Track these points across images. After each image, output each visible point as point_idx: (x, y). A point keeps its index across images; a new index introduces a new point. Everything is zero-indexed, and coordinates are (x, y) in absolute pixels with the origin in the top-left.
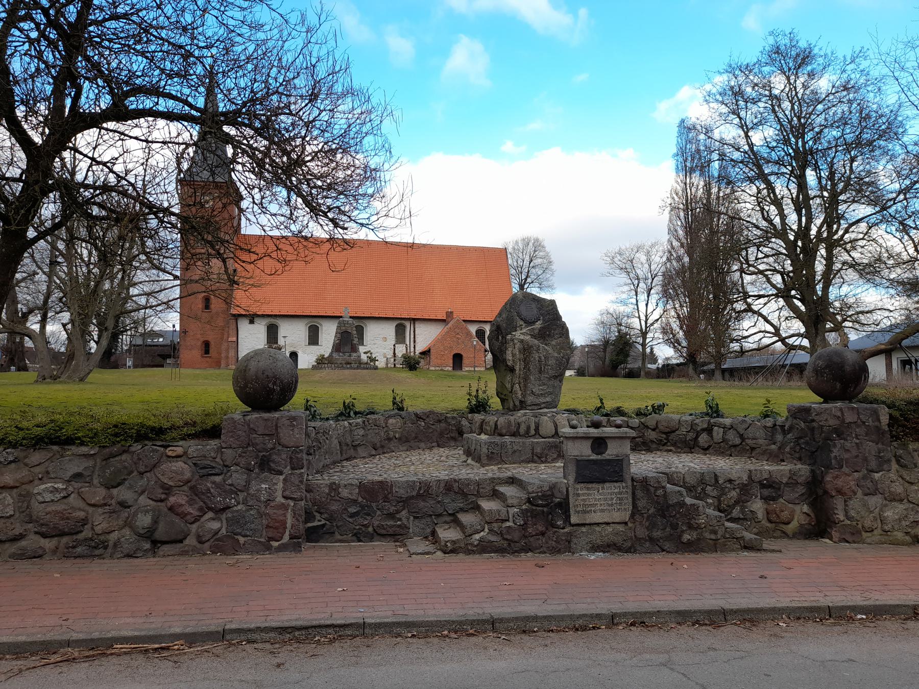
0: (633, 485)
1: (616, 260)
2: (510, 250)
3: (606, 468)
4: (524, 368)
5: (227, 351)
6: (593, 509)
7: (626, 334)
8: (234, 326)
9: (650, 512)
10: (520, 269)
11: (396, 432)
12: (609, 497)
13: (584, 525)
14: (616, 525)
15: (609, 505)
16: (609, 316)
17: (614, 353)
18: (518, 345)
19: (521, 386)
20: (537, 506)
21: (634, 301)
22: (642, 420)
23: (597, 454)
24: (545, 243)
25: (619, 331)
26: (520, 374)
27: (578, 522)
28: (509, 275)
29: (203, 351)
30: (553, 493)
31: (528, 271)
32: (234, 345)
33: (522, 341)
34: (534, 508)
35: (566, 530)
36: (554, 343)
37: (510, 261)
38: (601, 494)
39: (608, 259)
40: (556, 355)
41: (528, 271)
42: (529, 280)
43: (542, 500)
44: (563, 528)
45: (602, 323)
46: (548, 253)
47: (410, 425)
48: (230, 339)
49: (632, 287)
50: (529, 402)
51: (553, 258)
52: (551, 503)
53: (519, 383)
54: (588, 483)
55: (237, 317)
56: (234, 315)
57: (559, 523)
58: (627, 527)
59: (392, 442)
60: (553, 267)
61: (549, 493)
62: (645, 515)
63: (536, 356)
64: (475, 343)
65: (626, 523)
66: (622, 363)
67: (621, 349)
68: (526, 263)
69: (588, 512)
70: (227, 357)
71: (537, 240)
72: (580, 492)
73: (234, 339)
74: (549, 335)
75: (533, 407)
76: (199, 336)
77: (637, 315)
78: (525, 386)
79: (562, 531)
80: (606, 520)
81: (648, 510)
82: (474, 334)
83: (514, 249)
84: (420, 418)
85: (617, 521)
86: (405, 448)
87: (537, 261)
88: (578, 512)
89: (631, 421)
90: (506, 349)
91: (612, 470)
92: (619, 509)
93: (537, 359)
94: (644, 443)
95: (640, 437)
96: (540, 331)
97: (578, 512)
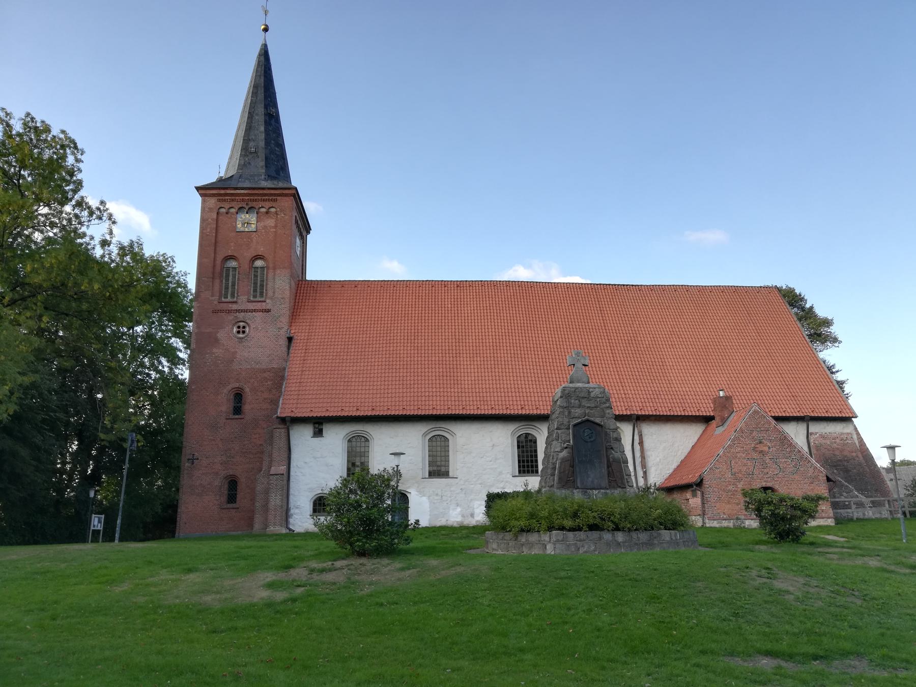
8: (282, 443)
29: (224, 499)
48: (273, 470)
56: (283, 420)
73: (283, 469)
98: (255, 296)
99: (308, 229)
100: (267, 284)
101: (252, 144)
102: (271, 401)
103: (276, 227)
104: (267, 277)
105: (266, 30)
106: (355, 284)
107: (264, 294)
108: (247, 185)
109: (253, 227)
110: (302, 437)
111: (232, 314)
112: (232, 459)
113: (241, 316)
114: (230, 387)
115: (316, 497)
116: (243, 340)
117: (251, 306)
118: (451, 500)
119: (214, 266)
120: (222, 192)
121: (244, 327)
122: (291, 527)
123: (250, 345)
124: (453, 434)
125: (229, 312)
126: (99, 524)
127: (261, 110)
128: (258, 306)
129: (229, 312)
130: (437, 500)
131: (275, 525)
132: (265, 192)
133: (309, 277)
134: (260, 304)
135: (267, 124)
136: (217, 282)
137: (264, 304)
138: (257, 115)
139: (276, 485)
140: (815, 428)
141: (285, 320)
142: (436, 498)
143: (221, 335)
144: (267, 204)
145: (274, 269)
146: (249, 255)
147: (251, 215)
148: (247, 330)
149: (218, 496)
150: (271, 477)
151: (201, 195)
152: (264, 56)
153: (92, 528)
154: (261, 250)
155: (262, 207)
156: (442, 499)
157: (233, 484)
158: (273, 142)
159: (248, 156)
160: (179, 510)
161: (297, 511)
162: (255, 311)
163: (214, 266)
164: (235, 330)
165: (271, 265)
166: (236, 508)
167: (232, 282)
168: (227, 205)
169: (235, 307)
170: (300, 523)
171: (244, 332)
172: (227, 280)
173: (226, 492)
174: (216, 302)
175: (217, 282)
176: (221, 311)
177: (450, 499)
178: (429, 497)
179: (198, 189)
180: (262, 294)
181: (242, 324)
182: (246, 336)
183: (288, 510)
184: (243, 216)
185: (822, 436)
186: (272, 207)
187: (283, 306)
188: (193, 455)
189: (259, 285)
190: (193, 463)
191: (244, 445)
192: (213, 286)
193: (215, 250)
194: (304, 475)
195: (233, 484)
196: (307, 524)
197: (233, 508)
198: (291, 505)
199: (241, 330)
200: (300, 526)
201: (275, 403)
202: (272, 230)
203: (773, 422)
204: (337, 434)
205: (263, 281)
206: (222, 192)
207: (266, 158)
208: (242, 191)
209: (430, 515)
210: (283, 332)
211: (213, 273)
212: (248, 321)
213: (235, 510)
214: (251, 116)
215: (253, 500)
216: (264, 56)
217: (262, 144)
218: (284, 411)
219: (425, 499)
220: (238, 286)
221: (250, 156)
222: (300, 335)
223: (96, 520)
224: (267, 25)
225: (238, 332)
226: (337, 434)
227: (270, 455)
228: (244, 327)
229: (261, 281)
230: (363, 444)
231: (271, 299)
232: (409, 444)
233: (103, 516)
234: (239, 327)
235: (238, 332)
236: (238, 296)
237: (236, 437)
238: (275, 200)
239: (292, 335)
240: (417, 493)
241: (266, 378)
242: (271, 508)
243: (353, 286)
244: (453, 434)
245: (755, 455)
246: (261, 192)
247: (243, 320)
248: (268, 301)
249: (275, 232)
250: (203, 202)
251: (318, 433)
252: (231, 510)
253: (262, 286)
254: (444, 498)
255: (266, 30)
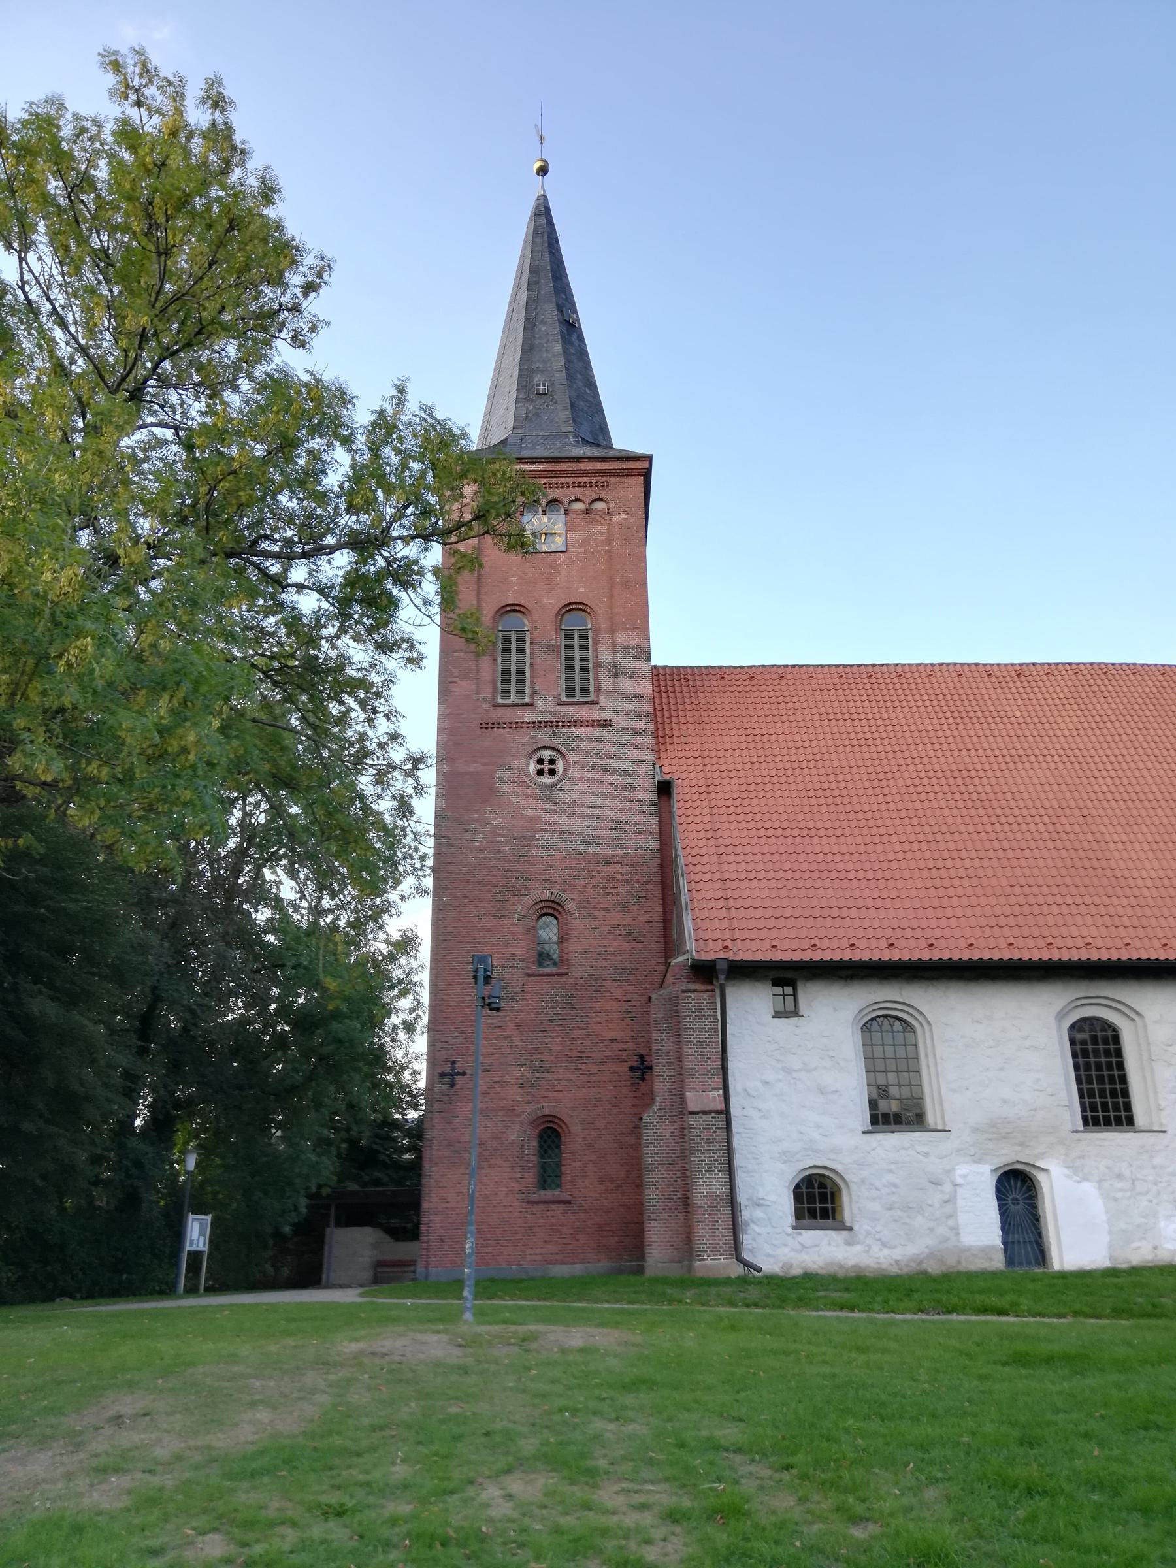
29: (531, 1177)
98: (570, 693)
100: (597, 666)
102: (630, 933)
103: (609, 541)
104: (595, 650)
105: (543, 171)
106: (781, 673)
107: (592, 689)
108: (540, 452)
111: (524, 730)
112: (547, 1076)
113: (544, 735)
114: (529, 899)
115: (801, 1176)
116: (554, 790)
117: (567, 713)
118: (1159, 1193)
121: (552, 761)
122: (747, 1256)
123: (569, 800)
124: (1133, 1016)
125: (518, 726)
126: (202, 1238)
127: (549, 312)
128: (583, 713)
129: (518, 726)
130: (1121, 1190)
131: (715, 1251)
132: (582, 466)
134: (585, 708)
137: (595, 707)
138: (543, 322)
139: (708, 1142)
141: (646, 743)
142: (1120, 1185)
143: (501, 778)
144: (588, 494)
145: (613, 631)
146: (555, 601)
147: (554, 518)
148: (560, 766)
149: (518, 1169)
150: (692, 1119)
152: (543, 215)
153: (188, 1248)
155: (577, 500)
156: (1133, 1189)
158: (579, 376)
159: (532, 401)
160: (425, 1205)
161: (759, 1213)
162: (575, 724)
164: (533, 767)
165: (604, 625)
166: (564, 1202)
167: (518, 662)
169: (529, 715)
170: (768, 1249)
171: (552, 772)
173: (534, 1159)
174: (486, 706)
176: (500, 725)
177: (1155, 1189)
178: (1100, 1181)
180: (585, 690)
181: (547, 754)
182: (560, 781)
183: (734, 1207)
186: (599, 500)
187: (639, 713)
188: (453, 1063)
189: (577, 668)
190: (453, 1085)
191: (573, 1040)
192: (478, 671)
193: (478, 593)
194: (763, 1117)
196: (786, 1250)
197: (559, 1202)
198: (742, 1197)
199: (546, 767)
200: (769, 1256)
202: (600, 548)
204: (835, 1010)
205: (587, 659)
207: (572, 405)
208: (533, 467)
209: (1110, 1233)
210: (643, 772)
212: (560, 747)
213: (562, 1207)
214: (530, 325)
216: (543, 215)
217: (560, 376)
219: (1088, 1188)
220: (532, 670)
221: (539, 402)
223: (196, 1226)
224: (545, 161)
225: (540, 773)
226: (835, 1010)
228: (552, 761)
229: (581, 660)
230: (900, 1038)
231: (609, 695)
232: (1026, 1038)
233: (209, 1218)
234: (540, 761)
235: (540, 773)
236: (534, 692)
237: (551, 1021)
238: (605, 485)
239: (667, 777)
240: (1067, 1172)
241: (613, 877)
242: (700, 1203)
243: (776, 676)
244: (1133, 1016)
246: (574, 466)
247: (549, 744)
248: (603, 702)
249: (609, 551)
252: (554, 1207)
253: (585, 671)
254: (1140, 1187)
255: (543, 171)
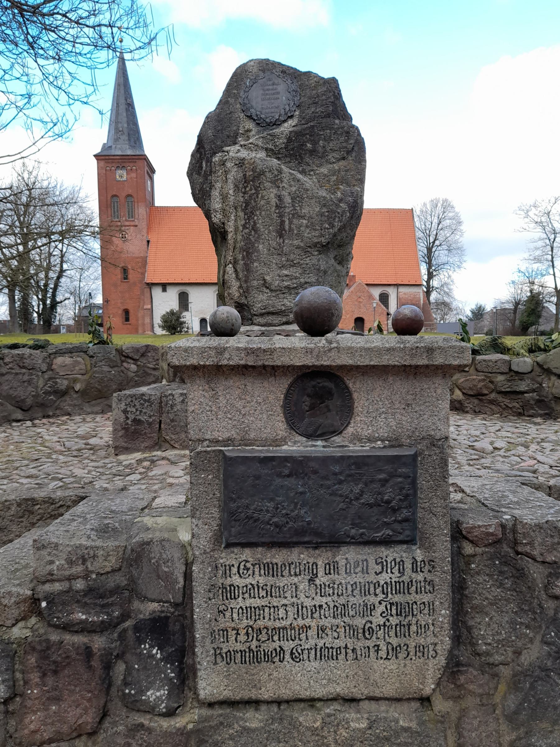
0: (457, 553)
1: (531, 214)
2: (417, 212)
3: (345, 489)
4: (244, 227)
5: (143, 317)
6: (288, 646)
7: (539, 294)
8: (148, 295)
9: (527, 658)
10: (428, 232)
11: (75, 381)
12: (357, 600)
13: (255, 703)
14: (383, 706)
15: (352, 630)
16: (520, 274)
17: (525, 314)
18: (234, 174)
19: (239, 267)
20: (67, 627)
21: (550, 257)
22: (539, 359)
23: (310, 436)
24: (454, 203)
25: (531, 291)
26: (235, 242)
27: (226, 694)
28: (415, 240)
29: (124, 319)
30: (132, 580)
31: (437, 234)
32: (149, 313)
33: (241, 163)
34: (54, 637)
35: (179, 722)
36: (324, 170)
37: (417, 224)
38: (321, 591)
39: (522, 213)
40: (323, 193)
41: (437, 234)
42: (437, 243)
43: (85, 607)
44: (170, 713)
45: (513, 282)
46: (457, 213)
47: (106, 369)
48: (145, 307)
49: (547, 241)
50: (257, 308)
51: (463, 218)
52: (125, 616)
53: (235, 263)
54: (271, 545)
55: (151, 285)
56: (148, 284)
57: (152, 695)
58: (427, 715)
59: (67, 398)
60: (462, 228)
61: (120, 580)
62: (505, 671)
63: (271, 194)
64: (375, 305)
65: (425, 701)
66: (533, 324)
67: (533, 310)
68: (435, 225)
69: (269, 658)
70: (144, 324)
71: (445, 201)
72: (236, 580)
73: (149, 307)
74: (313, 152)
75: (270, 319)
76: (120, 305)
77: (552, 273)
78: (247, 268)
79: (165, 724)
80: (339, 689)
81: (518, 653)
82: (378, 298)
83: (422, 211)
84: (128, 357)
85: (389, 690)
86: (98, 408)
87: (447, 222)
88: (229, 658)
89: (515, 360)
90: (211, 187)
91: (367, 498)
92: (396, 650)
93: (274, 201)
94: (540, 402)
95: (533, 391)
96: (289, 140)
97: (229, 658)
99: (153, 171)
101: (120, 125)
103: (137, 178)
109: (125, 178)
110: (157, 292)
119: (107, 201)
120: (107, 157)
133: (157, 204)
135: (127, 110)
136: (109, 209)
140: (402, 290)
151: (97, 159)
154: (130, 192)
157: (127, 312)
163: (107, 201)
168: (110, 165)
172: (114, 208)
175: (109, 209)
179: (95, 156)
184: (119, 172)
185: (405, 294)
195: (127, 312)
201: (143, 274)
203: (365, 286)
206: (107, 157)
210: (144, 237)
211: (107, 205)
215: (137, 320)
218: (148, 280)
221: (120, 133)
222: (153, 238)
227: (144, 300)
245: (356, 303)
250: (98, 163)
251: (164, 290)
